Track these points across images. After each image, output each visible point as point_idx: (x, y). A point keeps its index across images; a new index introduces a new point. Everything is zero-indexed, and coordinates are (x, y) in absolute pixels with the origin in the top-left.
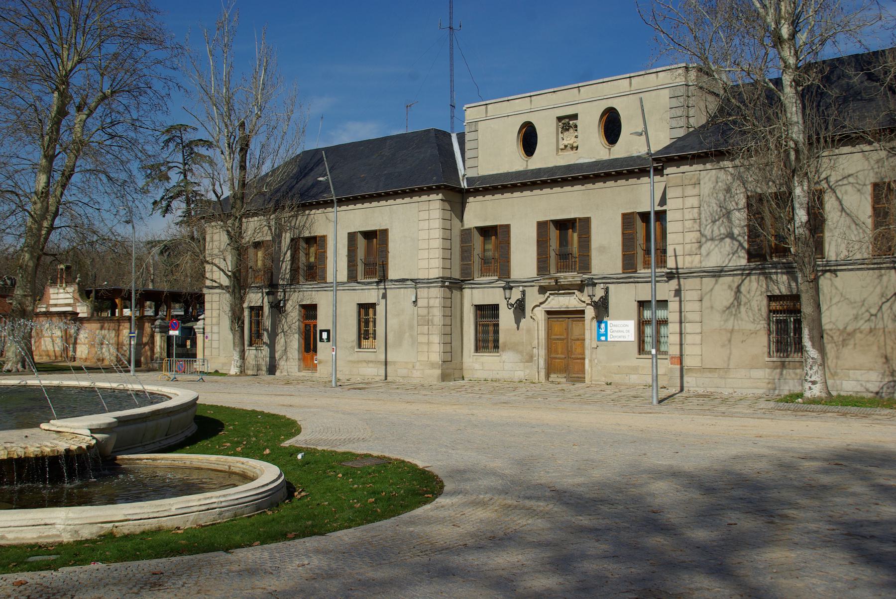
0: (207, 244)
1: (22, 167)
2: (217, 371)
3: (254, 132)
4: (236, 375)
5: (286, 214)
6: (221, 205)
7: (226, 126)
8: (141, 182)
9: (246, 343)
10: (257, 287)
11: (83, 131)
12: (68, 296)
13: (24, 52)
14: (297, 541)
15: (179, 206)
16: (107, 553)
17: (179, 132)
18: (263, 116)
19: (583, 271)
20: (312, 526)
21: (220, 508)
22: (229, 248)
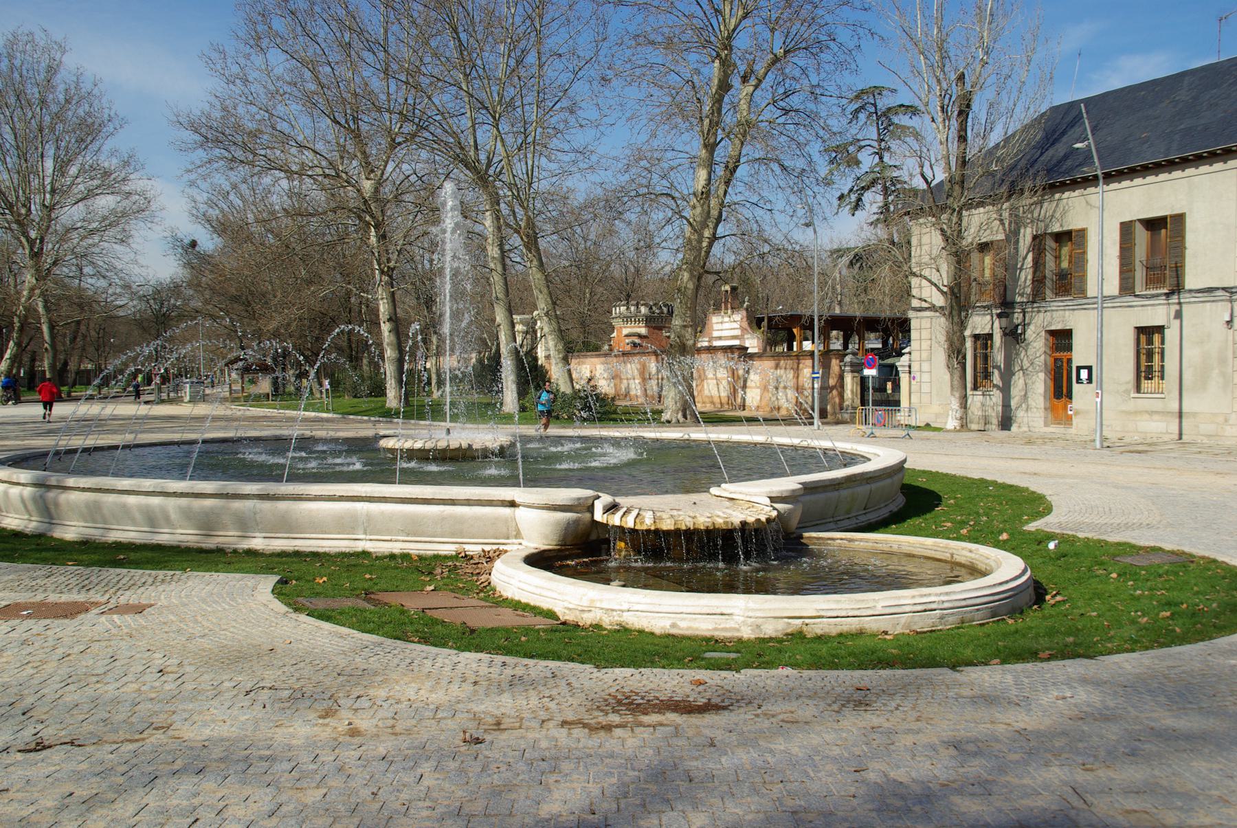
0: (913, 249)
1: (678, 161)
2: (928, 425)
3: (978, 86)
4: (955, 430)
5: (1026, 201)
7: (939, 81)
8: (823, 170)
10: (984, 307)
11: (749, 108)
12: (736, 325)
13: (679, 14)
14: (1053, 663)
15: (874, 200)
16: (798, 657)
17: (872, 97)
20: (1075, 644)
22: (944, 253)
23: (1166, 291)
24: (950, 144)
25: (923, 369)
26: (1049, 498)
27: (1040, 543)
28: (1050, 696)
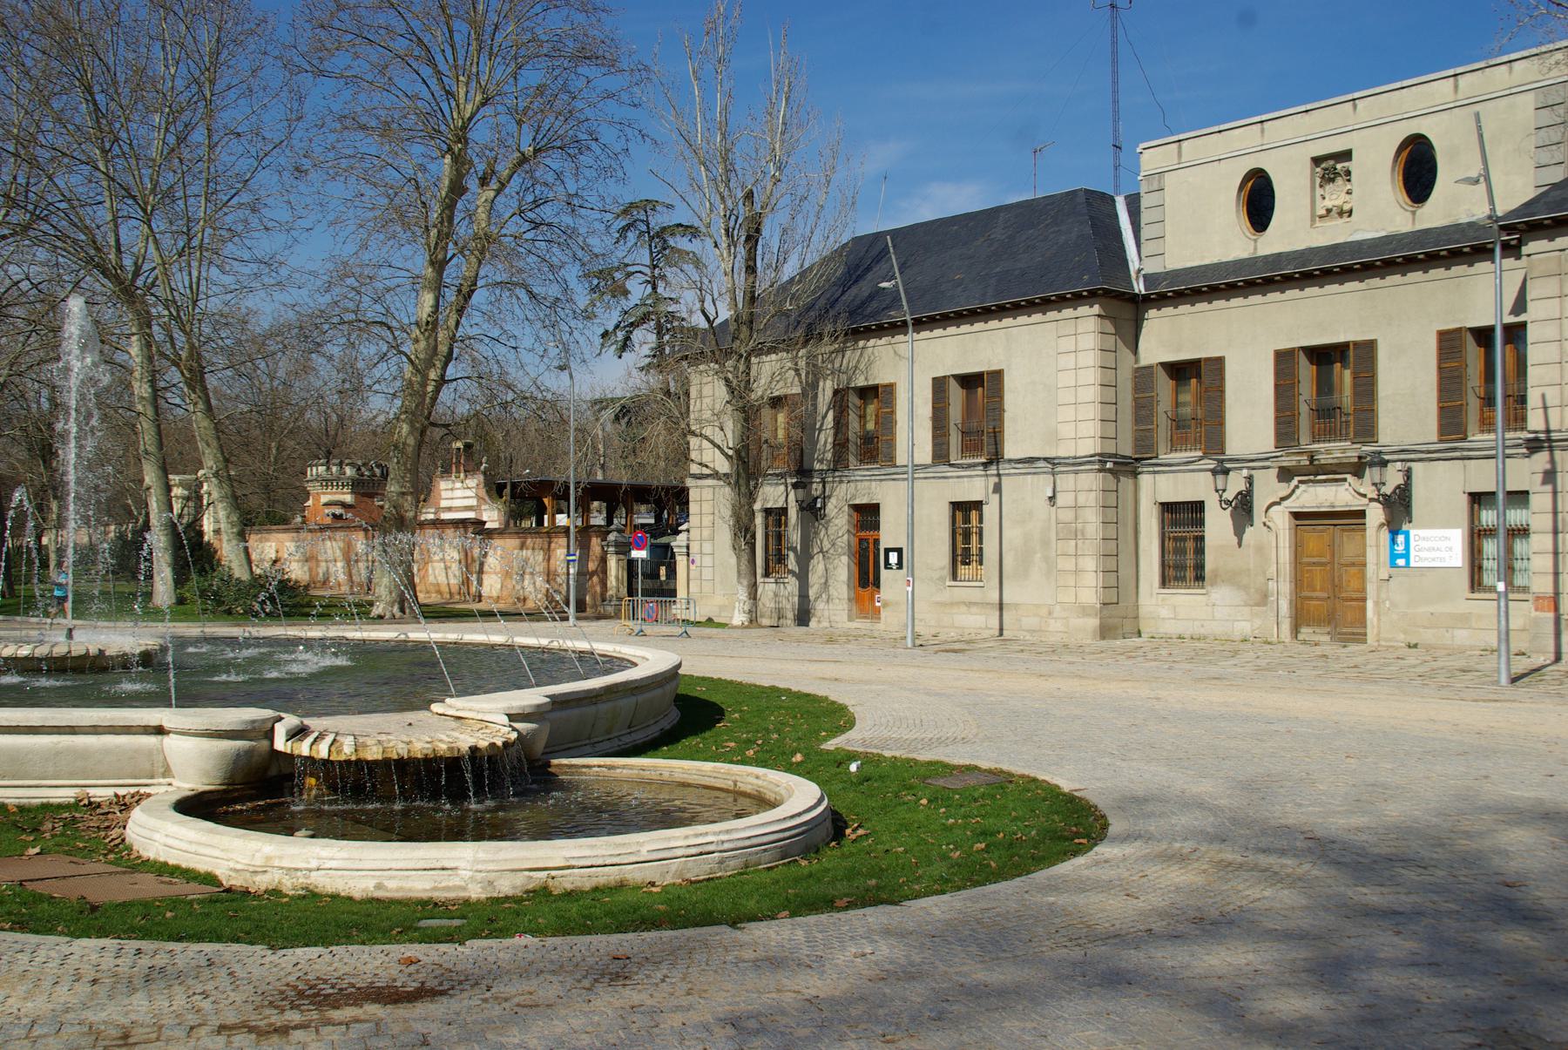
4: (743, 627)
5: (826, 348)
7: (723, 198)
9: (759, 571)
10: (777, 475)
18: (784, 179)
19: (1362, 440)
20: (878, 887)
21: (721, 851)
23: (984, 460)
24: (736, 276)
27: (839, 765)
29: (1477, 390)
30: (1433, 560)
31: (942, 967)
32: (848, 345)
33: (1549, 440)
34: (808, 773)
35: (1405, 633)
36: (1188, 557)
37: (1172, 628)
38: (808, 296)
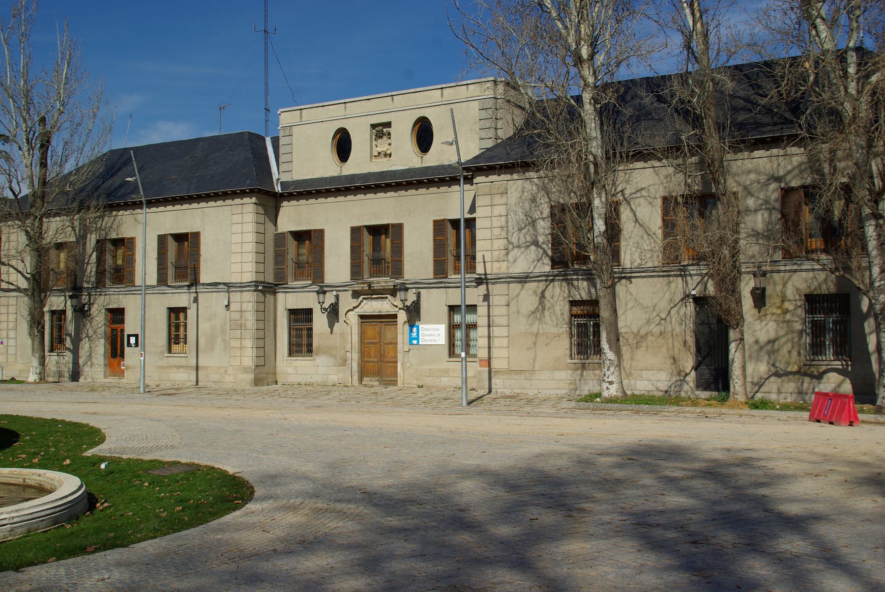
4: (35, 383)
5: (92, 215)
6: (18, 203)
7: (25, 120)
9: (47, 348)
10: (59, 290)
18: (66, 112)
19: (396, 276)
20: (115, 538)
21: (12, 524)
23: (188, 284)
24: (33, 168)
25: (10, 336)
26: (103, 431)
27: (94, 465)
28: (93, 580)
29: (452, 252)
30: (431, 341)
31: (152, 582)
32: (106, 213)
33: (486, 279)
34: (74, 471)
35: (417, 379)
36: (303, 339)
37: (294, 379)
38: (81, 183)
